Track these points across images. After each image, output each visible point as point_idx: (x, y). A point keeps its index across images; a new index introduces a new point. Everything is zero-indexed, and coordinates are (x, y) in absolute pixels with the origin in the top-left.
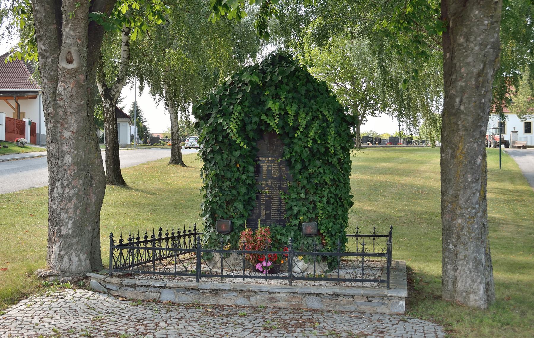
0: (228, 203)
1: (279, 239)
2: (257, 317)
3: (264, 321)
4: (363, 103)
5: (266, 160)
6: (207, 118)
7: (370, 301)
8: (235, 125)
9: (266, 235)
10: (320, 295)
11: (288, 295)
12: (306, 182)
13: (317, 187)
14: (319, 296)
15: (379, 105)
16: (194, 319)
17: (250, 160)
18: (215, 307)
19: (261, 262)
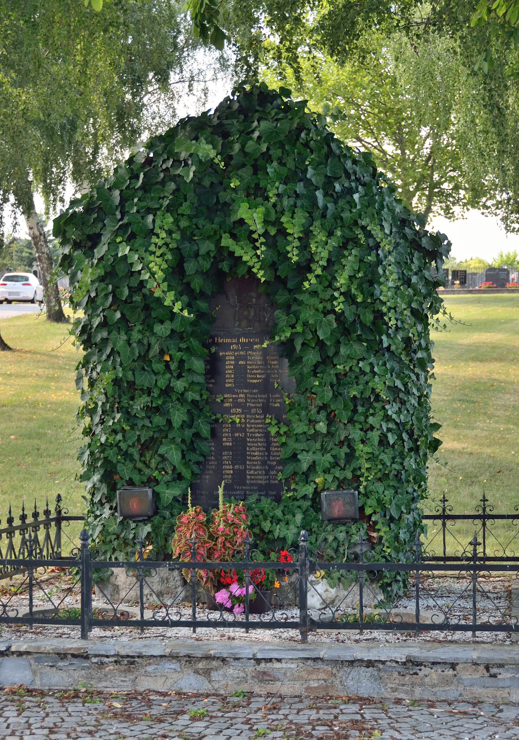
0: (145, 447)
1: (267, 530)
2: (232, 718)
3: (250, 729)
4: (423, 189)
5: (232, 344)
6: (89, 244)
7: (494, 676)
8: (159, 260)
9: (236, 521)
10: (376, 664)
11: (301, 665)
12: (331, 394)
13: (355, 406)
14: (373, 666)
15: (462, 192)
16: (87, 728)
17: (195, 343)
18: (130, 697)
19: (227, 586)
